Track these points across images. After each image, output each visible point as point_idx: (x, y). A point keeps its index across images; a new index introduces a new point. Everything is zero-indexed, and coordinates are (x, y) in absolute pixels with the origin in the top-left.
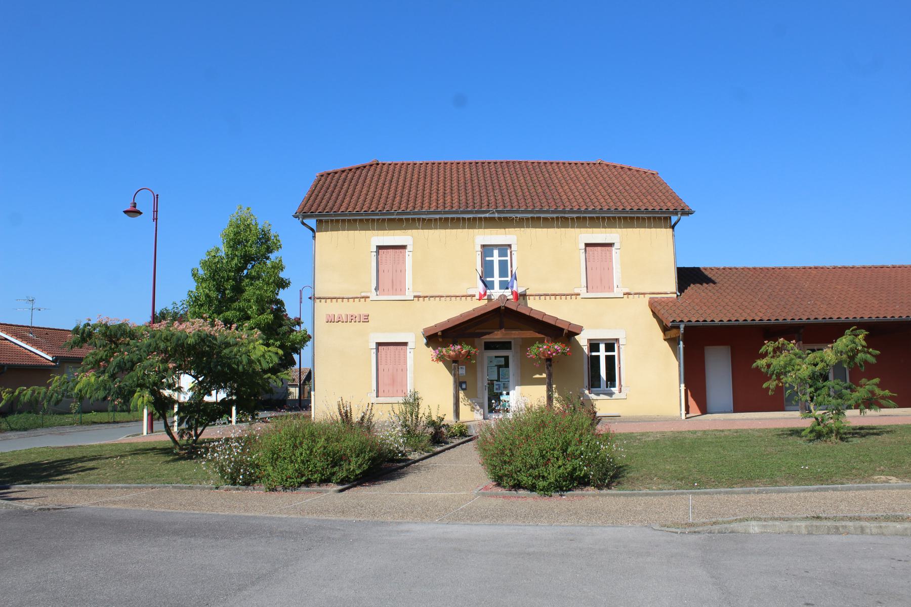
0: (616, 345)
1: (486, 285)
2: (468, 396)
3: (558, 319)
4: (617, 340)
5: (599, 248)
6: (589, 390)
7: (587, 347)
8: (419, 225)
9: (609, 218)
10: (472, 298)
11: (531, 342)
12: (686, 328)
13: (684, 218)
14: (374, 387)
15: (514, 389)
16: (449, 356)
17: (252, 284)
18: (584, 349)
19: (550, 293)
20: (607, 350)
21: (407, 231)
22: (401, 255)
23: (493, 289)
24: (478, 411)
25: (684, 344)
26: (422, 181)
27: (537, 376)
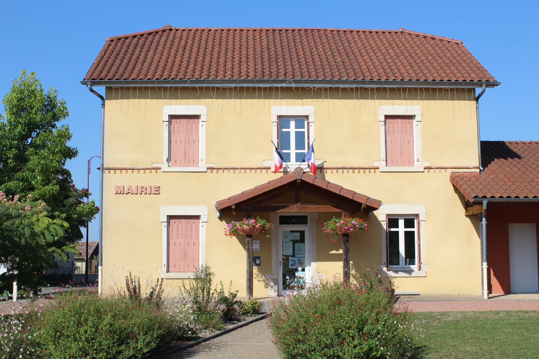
0: (415, 221)
1: (282, 158)
4: (417, 216)
6: (387, 267)
7: (385, 222)
8: (213, 93)
9: (410, 89)
10: (267, 171)
11: (328, 217)
12: (489, 204)
13: (489, 90)
16: (243, 231)
18: (383, 225)
23: (290, 162)
24: (272, 287)
25: (487, 220)
27: (334, 252)
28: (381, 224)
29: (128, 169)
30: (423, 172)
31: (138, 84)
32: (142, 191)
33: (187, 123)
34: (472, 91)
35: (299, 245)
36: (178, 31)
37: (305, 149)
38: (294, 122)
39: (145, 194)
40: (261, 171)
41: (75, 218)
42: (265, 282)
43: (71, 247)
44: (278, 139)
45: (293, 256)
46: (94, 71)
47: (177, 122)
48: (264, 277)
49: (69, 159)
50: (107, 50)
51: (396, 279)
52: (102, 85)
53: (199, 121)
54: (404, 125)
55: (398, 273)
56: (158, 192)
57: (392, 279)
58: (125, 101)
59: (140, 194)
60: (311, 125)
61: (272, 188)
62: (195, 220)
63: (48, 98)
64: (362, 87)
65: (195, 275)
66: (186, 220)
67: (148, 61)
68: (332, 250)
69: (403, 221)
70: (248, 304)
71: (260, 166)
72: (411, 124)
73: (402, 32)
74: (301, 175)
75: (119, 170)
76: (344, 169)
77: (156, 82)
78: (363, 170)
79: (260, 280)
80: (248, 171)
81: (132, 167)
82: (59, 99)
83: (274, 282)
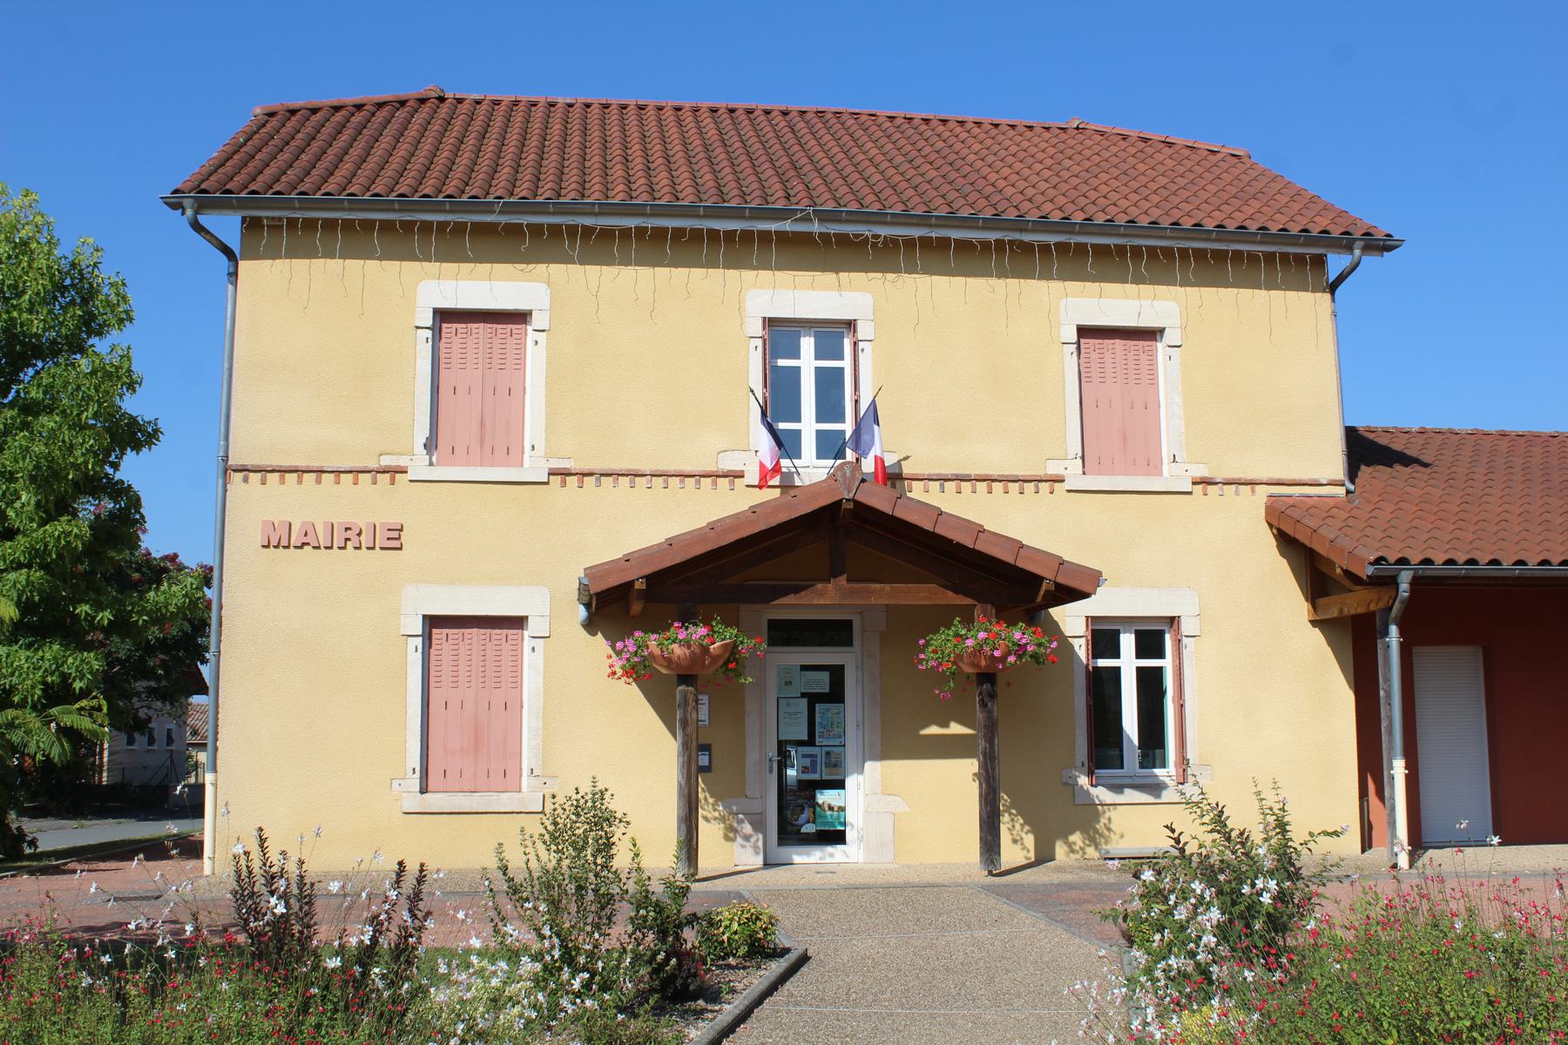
0: (1167, 637)
1: (779, 442)
2: (719, 796)
3: (1022, 546)
4: (1172, 621)
5: (1119, 344)
6: (1090, 773)
7: (1083, 641)
8: (573, 245)
9: (1152, 251)
10: (732, 483)
11: (939, 618)
12: (1415, 582)
13: (1370, 262)
14: (414, 760)
15: (861, 771)
16: (669, 662)
17: (25, 426)
18: (1077, 649)
19: (973, 471)
20: (1140, 654)
21: (532, 266)
22: (511, 341)
23: (799, 457)
24: (747, 838)
25: (1402, 633)
26: (575, 140)
27: (934, 730)
28: (1072, 647)
29: (304, 472)
30: (1190, 493)
31: (343, 209)
32: (347, 540)
33: (490, 336)
34: (1319, 262)
35: (828, 710)
36: (461, 103)
37: (844, 421)
38: (812, 339)
39: (356, 548)
40: (715, 483)
41: (141, 623)
42: (724, 823)
43: (82, 709)
44: (766, 387)
45: (811, 742)
46: (210, 175)
47: (459, 331)
48: (721, 808)
49: (134, 452)
50: (255, 133)
51: (1116, 812)
52: (231, 212)
53: (526, 330)
54: (1131, 357)
55: (1122, 792)
56: (396, 544)
57: (1104, 812)
58: (300, 265)
59: (340, 548)
60: (863, 350)
61: (763, 527)
62: (511, 632)
63: (73, 265)
64: (1016, 241)
65: (548, 823)
66: (483, 631)
67: (374, 159)
68: (927, 725)
69: (1133, 636)
70: (728, 923)
71: (711, 468)
72: (1150, 353)
73: (1077, 128)
74: (855, 487)
75: (277, 474)
76: (961, 480)
77: (397, 206)
78: (1017, 484)
79: (709, 816)
80: (674, 481)
81: (315, 464)
82: (106, 274)
83: (752, 823)
